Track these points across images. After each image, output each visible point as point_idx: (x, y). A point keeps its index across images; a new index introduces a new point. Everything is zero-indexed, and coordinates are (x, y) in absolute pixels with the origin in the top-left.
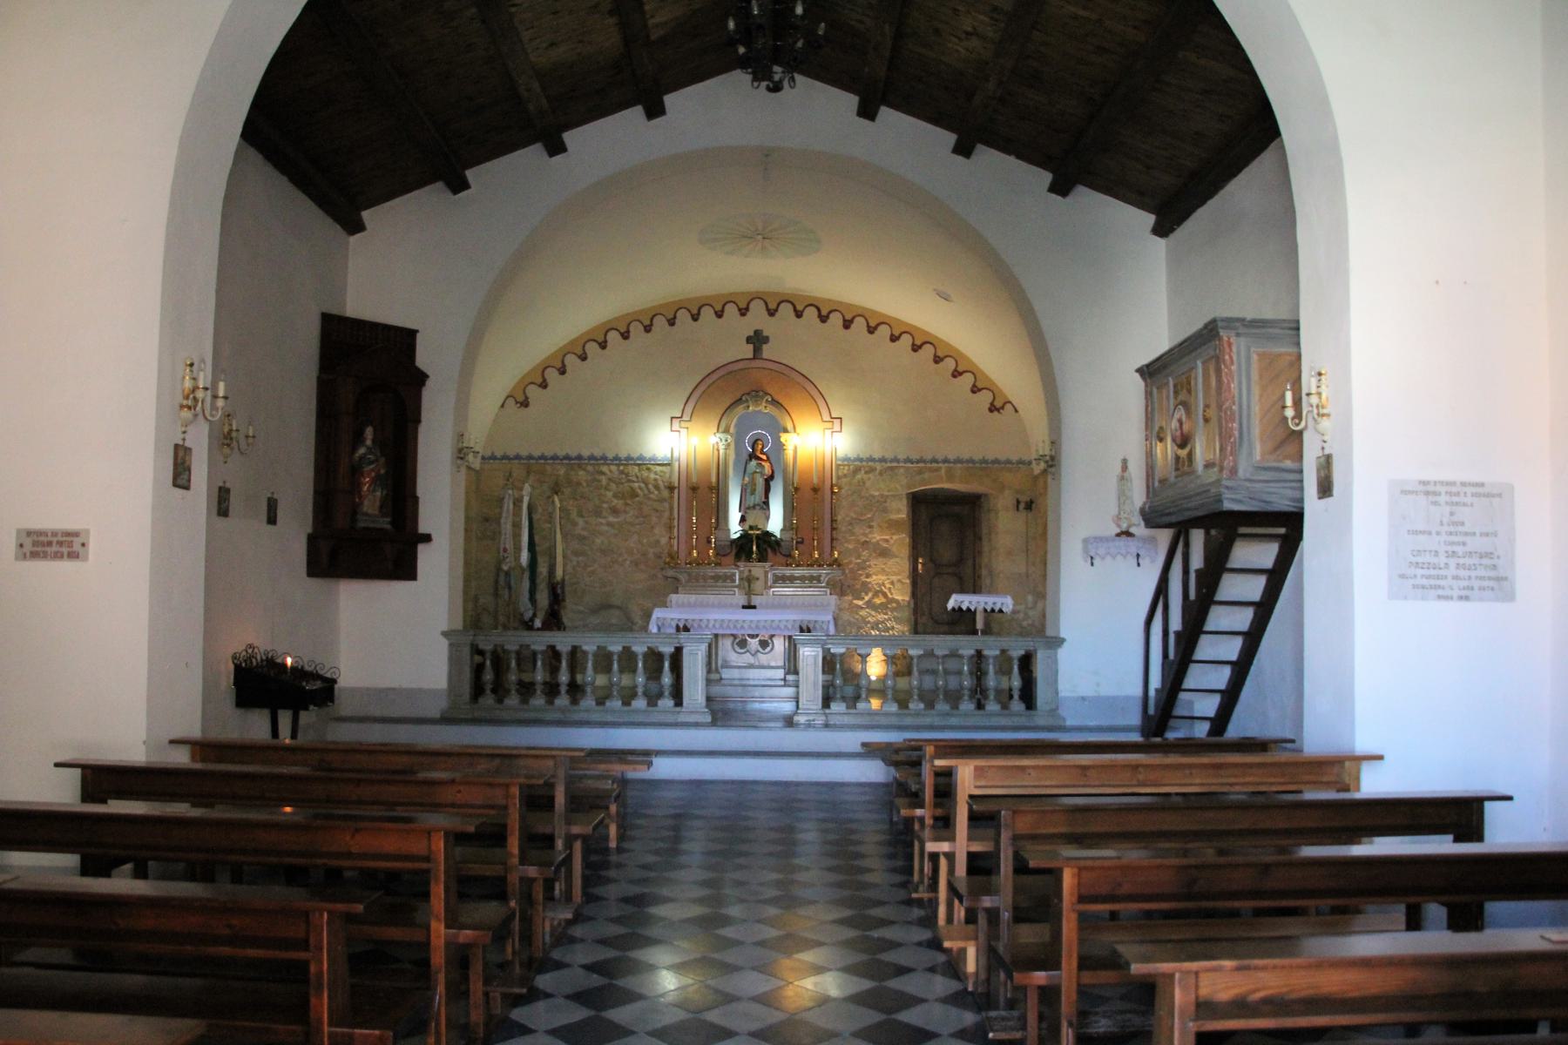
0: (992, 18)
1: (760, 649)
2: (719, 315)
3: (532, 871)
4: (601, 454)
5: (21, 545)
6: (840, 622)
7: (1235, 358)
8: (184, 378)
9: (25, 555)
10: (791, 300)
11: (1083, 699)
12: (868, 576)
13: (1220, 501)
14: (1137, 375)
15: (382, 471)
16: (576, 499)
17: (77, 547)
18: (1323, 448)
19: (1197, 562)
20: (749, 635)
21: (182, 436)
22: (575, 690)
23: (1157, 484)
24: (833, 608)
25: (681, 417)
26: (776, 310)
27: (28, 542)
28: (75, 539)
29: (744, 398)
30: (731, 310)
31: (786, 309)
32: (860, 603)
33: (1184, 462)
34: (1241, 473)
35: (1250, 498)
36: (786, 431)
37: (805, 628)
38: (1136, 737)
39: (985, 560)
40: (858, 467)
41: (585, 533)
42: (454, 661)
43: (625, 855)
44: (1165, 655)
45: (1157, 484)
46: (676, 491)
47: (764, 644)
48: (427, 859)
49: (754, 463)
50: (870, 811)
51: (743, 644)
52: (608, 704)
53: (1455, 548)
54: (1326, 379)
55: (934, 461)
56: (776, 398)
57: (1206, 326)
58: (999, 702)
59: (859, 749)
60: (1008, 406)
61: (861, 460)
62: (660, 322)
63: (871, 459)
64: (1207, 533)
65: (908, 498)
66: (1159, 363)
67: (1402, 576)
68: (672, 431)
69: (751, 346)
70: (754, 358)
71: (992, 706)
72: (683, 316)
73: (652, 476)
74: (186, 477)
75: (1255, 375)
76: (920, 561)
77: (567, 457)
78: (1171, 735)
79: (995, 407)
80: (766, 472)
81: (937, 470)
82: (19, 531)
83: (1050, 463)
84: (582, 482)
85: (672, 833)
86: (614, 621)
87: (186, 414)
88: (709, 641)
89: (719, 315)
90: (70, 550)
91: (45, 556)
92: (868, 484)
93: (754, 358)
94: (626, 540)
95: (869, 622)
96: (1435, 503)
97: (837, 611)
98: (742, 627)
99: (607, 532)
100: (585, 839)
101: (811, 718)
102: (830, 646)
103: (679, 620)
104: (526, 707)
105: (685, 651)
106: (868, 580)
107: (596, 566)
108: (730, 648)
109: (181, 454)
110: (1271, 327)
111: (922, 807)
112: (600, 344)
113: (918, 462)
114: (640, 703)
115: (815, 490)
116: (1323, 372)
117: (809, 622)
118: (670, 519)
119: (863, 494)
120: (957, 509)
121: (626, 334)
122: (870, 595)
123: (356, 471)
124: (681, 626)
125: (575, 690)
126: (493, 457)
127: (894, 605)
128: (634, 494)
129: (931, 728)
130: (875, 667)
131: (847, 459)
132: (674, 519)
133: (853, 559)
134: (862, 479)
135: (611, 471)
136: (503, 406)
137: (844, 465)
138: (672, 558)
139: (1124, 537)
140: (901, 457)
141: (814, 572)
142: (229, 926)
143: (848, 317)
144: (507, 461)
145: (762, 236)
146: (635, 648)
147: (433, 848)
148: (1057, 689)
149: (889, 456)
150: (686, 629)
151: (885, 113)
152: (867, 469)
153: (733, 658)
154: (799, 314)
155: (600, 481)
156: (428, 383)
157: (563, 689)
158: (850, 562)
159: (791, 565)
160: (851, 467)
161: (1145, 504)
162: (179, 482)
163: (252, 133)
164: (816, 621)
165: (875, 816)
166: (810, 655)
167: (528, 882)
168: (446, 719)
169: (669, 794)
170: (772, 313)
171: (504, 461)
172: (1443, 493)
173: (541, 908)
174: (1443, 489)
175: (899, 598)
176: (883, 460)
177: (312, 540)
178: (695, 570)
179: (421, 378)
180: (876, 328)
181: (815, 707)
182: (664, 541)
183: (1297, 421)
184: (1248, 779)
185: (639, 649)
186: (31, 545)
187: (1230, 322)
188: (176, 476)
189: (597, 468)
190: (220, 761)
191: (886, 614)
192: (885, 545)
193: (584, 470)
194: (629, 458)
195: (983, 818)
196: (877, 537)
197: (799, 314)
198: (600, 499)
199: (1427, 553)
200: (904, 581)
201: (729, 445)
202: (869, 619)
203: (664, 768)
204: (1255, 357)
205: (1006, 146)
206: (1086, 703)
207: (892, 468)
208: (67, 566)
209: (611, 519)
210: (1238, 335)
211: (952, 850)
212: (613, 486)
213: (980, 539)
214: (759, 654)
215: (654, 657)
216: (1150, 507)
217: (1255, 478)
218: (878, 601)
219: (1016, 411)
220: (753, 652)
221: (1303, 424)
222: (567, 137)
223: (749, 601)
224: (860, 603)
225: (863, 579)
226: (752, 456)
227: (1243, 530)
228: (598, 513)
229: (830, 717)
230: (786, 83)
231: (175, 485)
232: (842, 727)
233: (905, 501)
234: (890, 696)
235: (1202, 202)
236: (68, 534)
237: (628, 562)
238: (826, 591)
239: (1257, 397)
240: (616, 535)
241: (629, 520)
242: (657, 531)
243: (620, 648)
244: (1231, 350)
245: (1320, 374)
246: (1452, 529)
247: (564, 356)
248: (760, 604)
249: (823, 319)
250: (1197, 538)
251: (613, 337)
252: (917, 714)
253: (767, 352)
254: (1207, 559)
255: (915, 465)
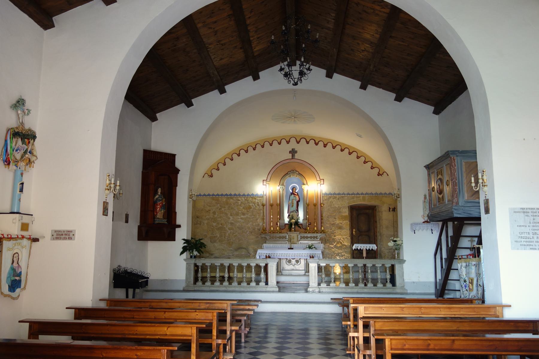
0: (371, 46)
1: (296, 264)
2: (280, 143)
3: (220, 341)
4: (238, 194)
5: (53, 235)
6: (325, 253)
7: (456, 164)
8: (107, 180)
9: (54, 238)
10: (314, 139)
11: (414, 282)
12: (335, 236)
13: (452, 213)
14: (425, 168)
15: (164, 203)
16: (230, 210)
17: (71, 236)
18: (485, 197)
19: (451, 233)
20: (292, 259)
21: (106, 199)
22: (230, 279)
23: (433, 206)
24: (322, 248)
25: (267, 180)
26: (300, 141)
27: (55, 234)
28: (70, 233)
29: (289, 173)
30: (284, 142)
31: (303, 141)
32: (332, 246)
33: (441, 199)
34: (460, 204)
35: (464, 213)
36: (304, 184)
37: (311, 256)
38: (433, 297)
39: (378, 230)
40: (330, 196)
41: (233, 222)
42: (188, 269)
43: (249, 338)
44: (442, 267)
45: (433, 206)
46: (265, 206)
47: (297, 261)
48: (191, 336)
49: (293, 196)
50: (335, 323)
51: (290, 261)
52: (242, 284)
53: (536, 231)
54: (485, 173)
55: (358, 194)
56: (300, 172)
57: (446, 153)
58: (382, 283)
59: (330, 301)
60: (385, 173)
61: (331, 194)
62: (259, 147)
63: (335, 194)
64: (454, 223)
65: (348, 208)
66: (431, 165)
67: (516, 241)
68: (263, 185)
69: (291, 154)
70: (292, 159)
71: (380, 285)
72: (267, 144)
73: (257, 201)
74: (107, 212)
75: (464, 169)
76: (354, 230)
77: (226, 195)
78: (446, 297)
79: (380, 174)
80: (297, 199)
81: (360, 197)
82: (52, 231)
83: (398, 197)
84: (232, 203)
85: (264, 331)
86: (243, 253)
87: (107, 192)
88: (277, 261)
89: (280, 143)
90: (69, 236)
91: (60, 239)
92: (334, 203)
93: (292, 159)
94: (248, 224)
95: (335, 253)
96: (527, 216)
97: (324, 249)
98: (289, 256)
99: (241, 221)
100: (236, 331)
101: (314, 289)
102: (320, 263)
103: (267, 254)
104: (213, 285)
105: (269, 265)
106: (335, 238)
107: (237, 233)
108: (285, 263)
109: (105, 204)
110: (469, 153)
111: (350, 321)
112: (237, 155)
113: (352, 194)
114: (253, 284)
115: (315, 205)
116: (485, 171)
117: (313, 254)
118: (263, 216)
119: (332, 206)
120: (367, 211)
121: (247, 151)
122: (336, 243)
123: (155, 204)
124: (267, 256)
125: (230, 279)
126: (200, 195)
127: (345, 247)
128: (250, 207)
129: (358, 293)
130: (338, 270)
131: (326, 194)
132: (264, 216)
133: (329, 230)
134: (332, 201)
135: (242, 199)
136: (203, 177)
137: (325, 196)
138: (264, 230)
139: (426, 223)
140: (346, 193)
141: (315, 235)
142: (136, 355)
143: (325, 143)
144: (205, 196)
145: (294, 117)
146: (243, 264)
147: (193, 332)
148: (404, 279)
149: (341, 192)
150: (269, 257)
151: (335, 75)
152: (333, 197)
153: (286, 267)
154: (308, 143)
155: (238, 203)
156: (180, 172)
157: (226, 279)
158: (328, 231)
159: (307, 233)
160: (328, 197)
161: (429, 213)
162: (105, 214)
163: (125, 98)
164: (315, 254)
165: (337, 325)
166: (313, 266)
167: (218, 345)
168: (184, 291)
169: (264, 317)
170: (298, 142)
171: (204, 196)
172: (530, 212)
173: (222, 354)
174: (530, 211)
175: (346, 244)
176: (339, 194)
177: (139, 227)
178: (272, 235)
179: (177, 171)
180: (335, 147)
181: (315, 285)
182: (261, 224)
183: (476, 188)
184: (461, 313)
185: (253, 265)
186: (56, 235)
187: (454, 152)
188: (104, 212)
189: (237, 198)
190: (115, 306)
191: (342, 250)
192: (341, 225)
193: (232, 199)
194: (248, 195)
195: (366, 326)
196: (337, 222)
197: (308, 143)
198: (238, 209)
199: (525, 233)
200: (348, 238)
201: (284, 189)
202: (336, 252)
203: (263, 308)
204: (464, 164)
205: (379, 85)
206: (415, 284)
207: (343, 197)
208: (68, 242)
209: (242, 216)
210: (457, 156)
211: (358, 336)
212: (243, 205)
213: (376, 222)
214: (295, 265)
215: (258, 267)
216: (430, 215)
217: (466, 205)
218: (338, 245)
219: (388, 175)
220: (293, 265)
221: (478, 188)
222: (227, 87)
223: (291, 246)
224: (332, 246)
225: (333, 237)
226: (292, 194)
227: (465, 222)
228: (237, 214)
229: (321, 289)
230: (299, 82)
231: (103, 215)
232: (325, 293)
233: (347, 209)
234: (342, 281)
235: (450, 103)
236: (69, 231)
237: (248, 232)
238: (320, 242)
239: (465, 178)
240: (244, 222)
241: (248, 217)
242: (258, 221)
243: (246, 264)
244: (454, 161)
245: (483, 171)
246: (534, 225)
247: (225, 159)
248: (296, 247)
249: (317, 144)
250: (450, 225)
251: (242, 152)
252: (352, 288)
253: (297, 156)
254: (454, 232)
255: (351, 196)
